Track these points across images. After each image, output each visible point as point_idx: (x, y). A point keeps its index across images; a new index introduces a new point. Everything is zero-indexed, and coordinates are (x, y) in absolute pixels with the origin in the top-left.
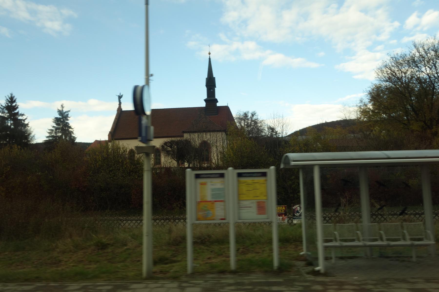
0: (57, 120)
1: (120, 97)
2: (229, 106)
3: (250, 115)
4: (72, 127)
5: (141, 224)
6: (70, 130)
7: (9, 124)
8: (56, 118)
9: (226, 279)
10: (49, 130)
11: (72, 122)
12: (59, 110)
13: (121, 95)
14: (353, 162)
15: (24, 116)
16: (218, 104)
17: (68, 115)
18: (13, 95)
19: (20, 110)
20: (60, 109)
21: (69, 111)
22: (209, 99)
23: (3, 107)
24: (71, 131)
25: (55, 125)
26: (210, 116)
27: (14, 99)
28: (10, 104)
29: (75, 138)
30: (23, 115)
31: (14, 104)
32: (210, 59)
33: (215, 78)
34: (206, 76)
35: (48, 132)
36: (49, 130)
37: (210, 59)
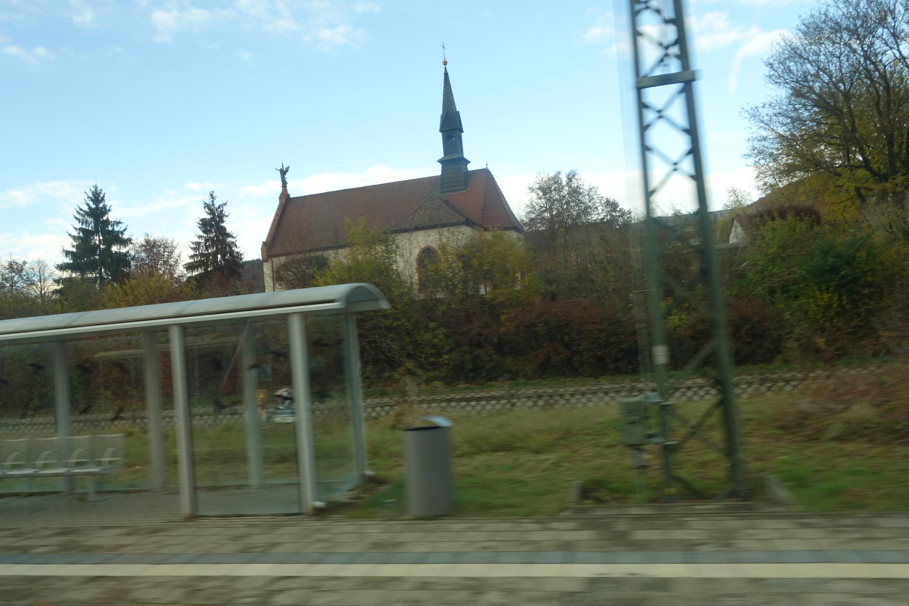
0: (205, 225)
1: (283, 172)
2: (202, 218)
3: (564, 181)
4: (234, 235)
5: (171, 424)
6: (229, 239)
7: (97, 242)
8: (202, 220)
9: (767, 514)
10: (193, 243)
11: (229, 225)
12: (206, 204)
13: (285, 167)
14: (146, 323)
15: (120, 225)
16: (470, 167)
17: (222, 211)
18: (99, 189)
19: (111, 217)
20: (209, 201)
21: (225, 204)
22: (448, 158)
23: (84, 211)
24: (233, 243)
25: (202, 234)
26: (452, 194)
27: (102, 196)
28: (93, 206)
29: (239, 256)
30: (119, 223)
31: (101, 205)
32: (446, 74)
33: (458, 112)
34: (439, 111)
35: (192, 248)
36: (193, 243)
37: (446, 74)
